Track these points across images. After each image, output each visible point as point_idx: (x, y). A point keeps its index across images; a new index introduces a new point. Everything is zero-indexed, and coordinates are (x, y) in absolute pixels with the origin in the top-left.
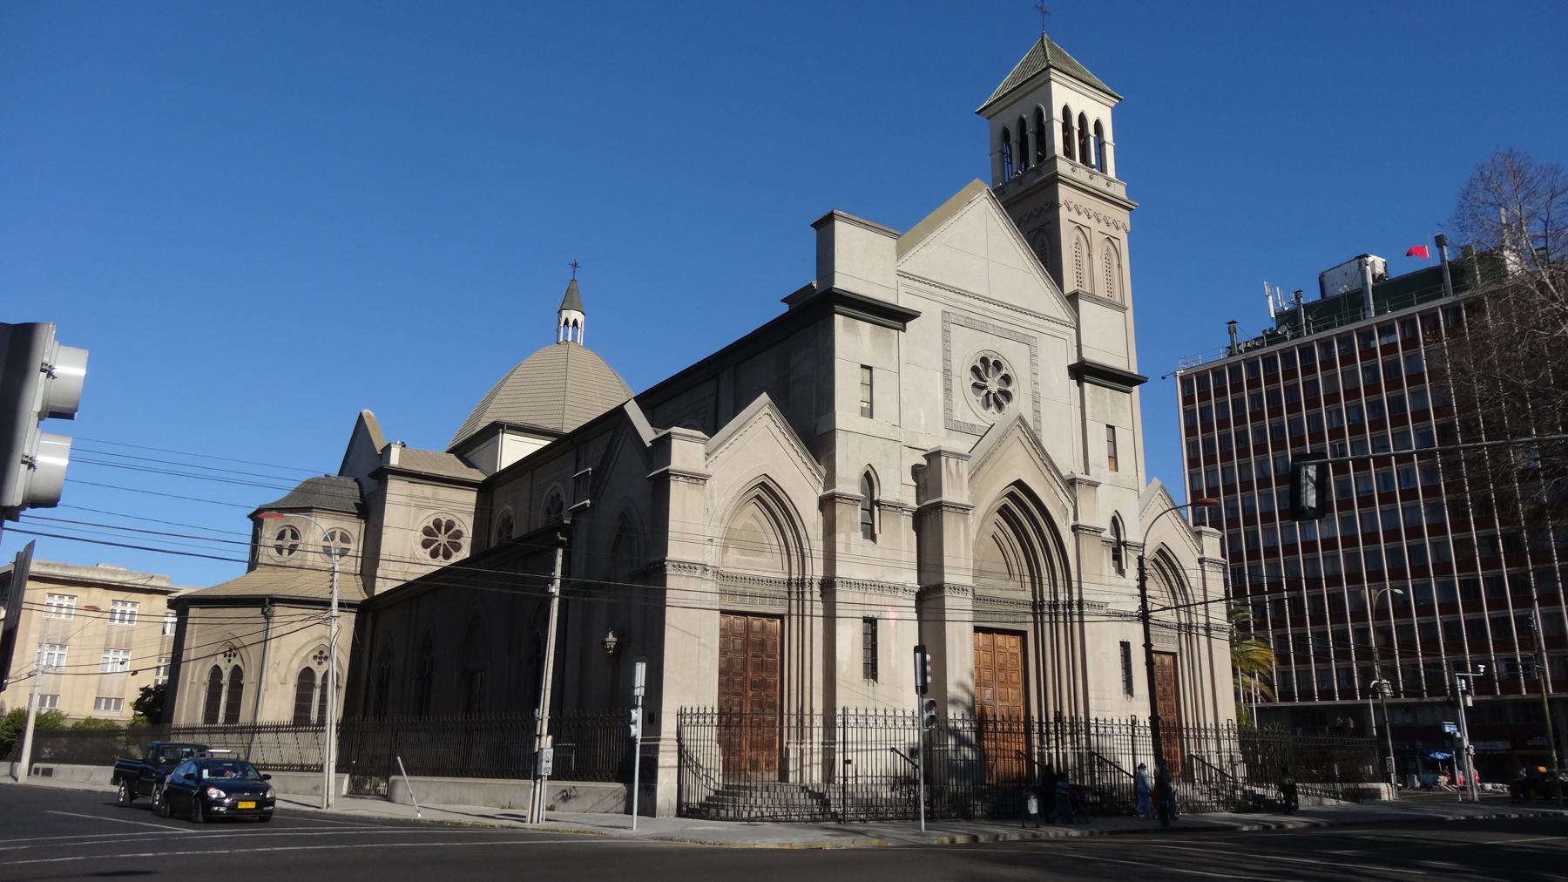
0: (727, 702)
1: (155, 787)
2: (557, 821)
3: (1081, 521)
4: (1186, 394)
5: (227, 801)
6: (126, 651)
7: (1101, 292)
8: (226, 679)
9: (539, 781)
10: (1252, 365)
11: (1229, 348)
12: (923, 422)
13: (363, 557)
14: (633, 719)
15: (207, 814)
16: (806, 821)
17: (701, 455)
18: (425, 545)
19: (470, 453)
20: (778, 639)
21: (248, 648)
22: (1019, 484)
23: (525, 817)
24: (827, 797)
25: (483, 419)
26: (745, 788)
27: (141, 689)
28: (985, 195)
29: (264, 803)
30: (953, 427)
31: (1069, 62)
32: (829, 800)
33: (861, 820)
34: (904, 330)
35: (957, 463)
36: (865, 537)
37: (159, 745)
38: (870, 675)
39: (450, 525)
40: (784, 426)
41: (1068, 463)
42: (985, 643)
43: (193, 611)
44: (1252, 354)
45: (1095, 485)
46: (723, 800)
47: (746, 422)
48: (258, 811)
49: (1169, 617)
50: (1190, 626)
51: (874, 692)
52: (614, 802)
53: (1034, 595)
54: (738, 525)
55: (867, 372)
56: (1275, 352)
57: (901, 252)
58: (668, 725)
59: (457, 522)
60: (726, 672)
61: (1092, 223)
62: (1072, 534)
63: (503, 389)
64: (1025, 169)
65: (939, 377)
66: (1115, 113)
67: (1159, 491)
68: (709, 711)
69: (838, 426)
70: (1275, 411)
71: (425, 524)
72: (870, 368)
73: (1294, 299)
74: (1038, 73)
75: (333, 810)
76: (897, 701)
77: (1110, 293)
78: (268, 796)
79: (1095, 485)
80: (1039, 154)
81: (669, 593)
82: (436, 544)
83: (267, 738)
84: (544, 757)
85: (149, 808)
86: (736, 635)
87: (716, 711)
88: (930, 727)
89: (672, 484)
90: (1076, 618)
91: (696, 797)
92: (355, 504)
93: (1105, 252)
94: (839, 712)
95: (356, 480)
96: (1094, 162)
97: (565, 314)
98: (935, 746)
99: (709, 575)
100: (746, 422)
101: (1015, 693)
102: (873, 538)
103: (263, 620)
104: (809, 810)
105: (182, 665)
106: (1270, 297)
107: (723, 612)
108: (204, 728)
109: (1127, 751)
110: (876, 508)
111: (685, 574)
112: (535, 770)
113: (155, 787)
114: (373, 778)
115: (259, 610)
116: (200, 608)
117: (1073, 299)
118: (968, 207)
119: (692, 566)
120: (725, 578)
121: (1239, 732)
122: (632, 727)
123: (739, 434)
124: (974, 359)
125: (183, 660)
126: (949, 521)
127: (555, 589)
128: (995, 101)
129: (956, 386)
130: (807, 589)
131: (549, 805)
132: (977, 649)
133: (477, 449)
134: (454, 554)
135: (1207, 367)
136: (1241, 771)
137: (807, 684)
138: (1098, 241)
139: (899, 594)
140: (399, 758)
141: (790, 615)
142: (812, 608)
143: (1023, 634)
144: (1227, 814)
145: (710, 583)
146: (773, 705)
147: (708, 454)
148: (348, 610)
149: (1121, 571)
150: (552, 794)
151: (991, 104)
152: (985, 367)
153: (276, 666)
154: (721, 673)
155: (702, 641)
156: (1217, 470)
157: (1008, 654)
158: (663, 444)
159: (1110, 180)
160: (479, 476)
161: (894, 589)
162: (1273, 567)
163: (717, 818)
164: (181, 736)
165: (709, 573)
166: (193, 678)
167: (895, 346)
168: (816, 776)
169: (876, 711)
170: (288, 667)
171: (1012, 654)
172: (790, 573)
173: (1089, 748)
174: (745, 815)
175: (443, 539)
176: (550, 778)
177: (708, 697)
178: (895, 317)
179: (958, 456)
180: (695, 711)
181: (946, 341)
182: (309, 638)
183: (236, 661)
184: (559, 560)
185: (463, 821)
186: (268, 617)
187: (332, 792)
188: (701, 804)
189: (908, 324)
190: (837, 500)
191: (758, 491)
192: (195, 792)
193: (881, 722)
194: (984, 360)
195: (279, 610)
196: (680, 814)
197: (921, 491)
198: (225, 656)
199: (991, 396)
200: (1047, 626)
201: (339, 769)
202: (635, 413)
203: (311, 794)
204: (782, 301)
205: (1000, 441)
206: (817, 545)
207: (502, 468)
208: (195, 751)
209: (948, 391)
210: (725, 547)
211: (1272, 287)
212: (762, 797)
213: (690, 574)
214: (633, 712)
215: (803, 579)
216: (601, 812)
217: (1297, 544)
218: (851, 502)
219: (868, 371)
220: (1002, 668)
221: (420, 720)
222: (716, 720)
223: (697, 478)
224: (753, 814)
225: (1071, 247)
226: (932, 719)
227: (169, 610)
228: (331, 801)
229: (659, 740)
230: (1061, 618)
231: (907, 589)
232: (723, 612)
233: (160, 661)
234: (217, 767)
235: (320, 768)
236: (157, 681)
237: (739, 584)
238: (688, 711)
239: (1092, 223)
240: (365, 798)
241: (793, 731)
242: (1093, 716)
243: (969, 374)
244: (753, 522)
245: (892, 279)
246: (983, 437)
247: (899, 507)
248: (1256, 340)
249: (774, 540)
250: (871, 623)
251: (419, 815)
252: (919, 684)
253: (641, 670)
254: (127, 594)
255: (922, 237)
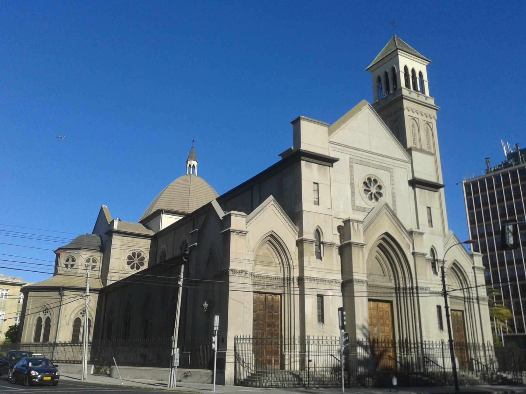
0: (257, 333)
1: (10, 370)
2: (181, 387)
3: (416, 250)
4: (468, 191)
5: (39, 376)
6: (3, 311)
7: (425, 147)
8: (43, 323)
9: (173, 368)
10: (497, 178)
11: (487, 170)
12: (342, 207)
13: (101, 271)
14: (213, 341)
15: (31, 383)
16: (292, 388)
17: (244, 223)
18: (128, 263)
19: (149, 223)
20: (279, 305)
21: (53, 309)
22: (387, 234)
23: (167, 385)
24: (301, 377)
25: (154, 208)
26: (264, 372)
27: (9, 327)
28: (368, 106)
29: (54, 377)
30: (356, 209)
31: (406, 47)
32: (302, 378)
33: (316, 387)
34: (332, 166)
35: (358, 225)
36: (317, 258)
37: (12, 352)
38: (321, 320)
39: (139, 255)
40: (279, 209)
41: (409, 224)
42: (374, 306)
43: (30, 293)
44: (497, 172)
45: (422, 234)
46: (254, 378)
47: (264, 208)
48: (52, 381)
49: (459, 294)
50: (469, 298)
51: (323, 328)
52: (207, 378)
53: (396, 284)
54: (261, 253)
55: (316, 185)
56: (499, 174)
57: (330, 133)
58: (230, 344)
59: (142, 253)
60: (256, 320)
61: (419, 116)
62: (412, 256)
63: (162, 195)
64: (388, 94)
65: (349, 187)
66: (428, 68)
67: (453, 236)
68: (248, 337)
69: (303, 209)
70: (509, 198)
71: (128, 254)
72: (317, 184)
73: (515, 147)
74: (393, 52)
75: (86, 381)
76: (333, 332)
77: (429, 147)
78: (56, 374)
79: (422, 234)
80: (394, 87)
81: (230, 284)
82: (133, 263)
83: (60, 348)
84: (175, 358)
85: (7, 380)
86: (260, 302)
87: (251, 337)
88: (346, 345)
89: (232, 236)
90: (415, 295)
91: (244, 376)
92: (99, 246)
93: (426, 129)
94: (306, 338)
95: (99, 236)
96: (419, 89)
97: (189, 162)
98: (350, 353)
99: (248, 276)
100: (264, 208)
101: (388, 329)
102: (321, 258)
103: (60, 297)
104: (293, 383)
105: (26, 316)
106: (504, 147)
107: (255, 292)
108: (34, 344)
109: (440, 356)
110: (322, 245)
111: (237, 275)
112: (172, 364)
113: (10, 370)
114: (104, 367)
115: (58, 292)
116: (33, 292)
117: (409, 151)
118: (360, 112)
119: (240, 272)
120: (255, 277)
121: (495, 348)
122: (213, 344)
123: (260, 213)
124: (365, 178)
125: (26, 314)
126: (355, 252)
127: (181, 283)
128: (374, 65)
129: (356, 191)
130: (292, 282)
131: (179, 380)
132: (370, 309)
133: (151, 221)
134: (141, 267)
135: (476, 179)
136: (496, 365)
137: (293, 325)
138: (422, 124)
139: (333, 284)
140: (114, 358)
141: (284, 294)
142: (294, 291)
143: (391, 302)
144: (488, 386)
145: (248, 279)
146: (277, 335)
147: (247, 222)
148: (93, 292)
149: (436, 273)
150: (180, 375)
151: (372, 66)
152: (369, 182)
153: (64, 317)
154: (254, 320)
155: (245, 305)
156: (483, 225)
157: (384, 311)
158: (227, 218)
159: (427, 98)
160: (152, 233)
161: (331, 281)
162: (512, 270)
163: (252, 386)
164: (24, 348)
165: (248, 274)
166: (30, 322)
167: (329, 173)
168: (297, 367)
169: (322, 337)
170: (70, 317)
171: (386, 311)
172: (284, 275)
173: (423, 355)
174: (264, 384)
175: (136, 260)
176: (178, 367)
177: (249, 331)
178: (328, 161)
179: (358, 221)
180: (242, 337)
181: (351, 171)
182: (79, 305)
183: (48, 315)
184: (182, 270)
185: (140, 386)
186: (61, 295)
187: (86, 373)
188: (245, 380)
189: (334, 164)
190: (304, 241)
191: (269, 238)
192: (26, 373)
193: (325, 342)
194: (369, 179)
195: (66, 293)
196: (235, 384)
197: (342, 237)
198: (43, 313)
199: (373, 195)
200: (402, 299)
201: (90, 363)
202: (216, 206)
203: (78, 374)
204: (279, 155)
205: (377, 214)
206: (296, 263)
207: (162, 229)
208: (28, 354)
209: (353, 193)
210: (255, 264)
211: (505, 142)
212: (272, 377)
213: (240, 275)
214: (213, 338)
215: (290, 277)
216: (201, 383)
217: (513, 261)
218: (310, 242)
219: (317, 185)
220: (382, 318)
221: (145, 340)
222: (251, 341)
223: (242, 233)
224: (268, 384)
225: (410, 127)
226: (347, 341)
227: (21, 293)
228: (85, 377)
229: (226, 350)
230: (408, 295)
231: (337, 281)
232: (255, 292)
233: (17, 314)
234: (36, 362)
235: (80, 362)
236: (16, 323)
237: (261, 280)
238: (239, 337)
239: (419, 116)
240: (101, 376)
241: (287, 346)
242: (424, 339)
243: (362, 185)
244: (267, 252)
245: (327, 145)
246: (369, 213)
247: (332, 245)
248: (499, 166)
249: (277, 261)
250: (321, 297)
251: (122, 384)
252: (341, 325)
253: (217, 318)
254: (4, 286)
255: (339, 126)
